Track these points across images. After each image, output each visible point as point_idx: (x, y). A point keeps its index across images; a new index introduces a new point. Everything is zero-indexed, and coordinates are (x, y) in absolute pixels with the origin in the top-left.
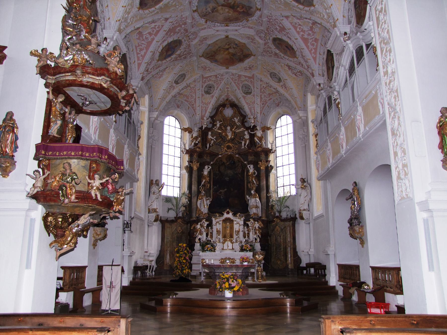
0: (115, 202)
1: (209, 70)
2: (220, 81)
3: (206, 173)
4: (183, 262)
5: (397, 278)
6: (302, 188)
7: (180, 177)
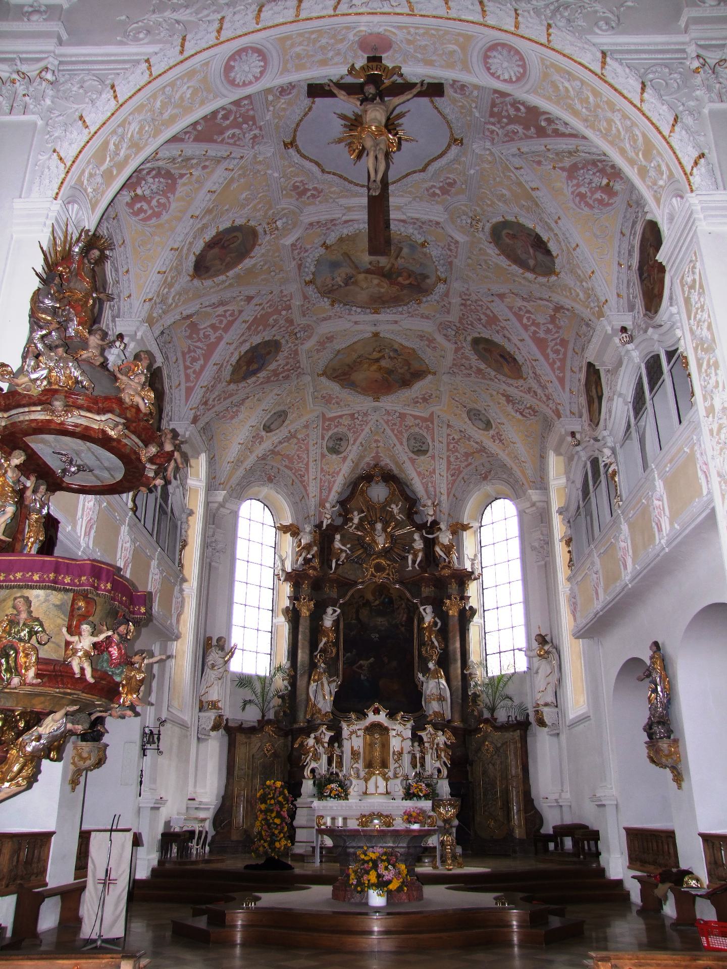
1: (338, 403)
2: (361, 425)
4: (275, 824)
6: (540, 656)
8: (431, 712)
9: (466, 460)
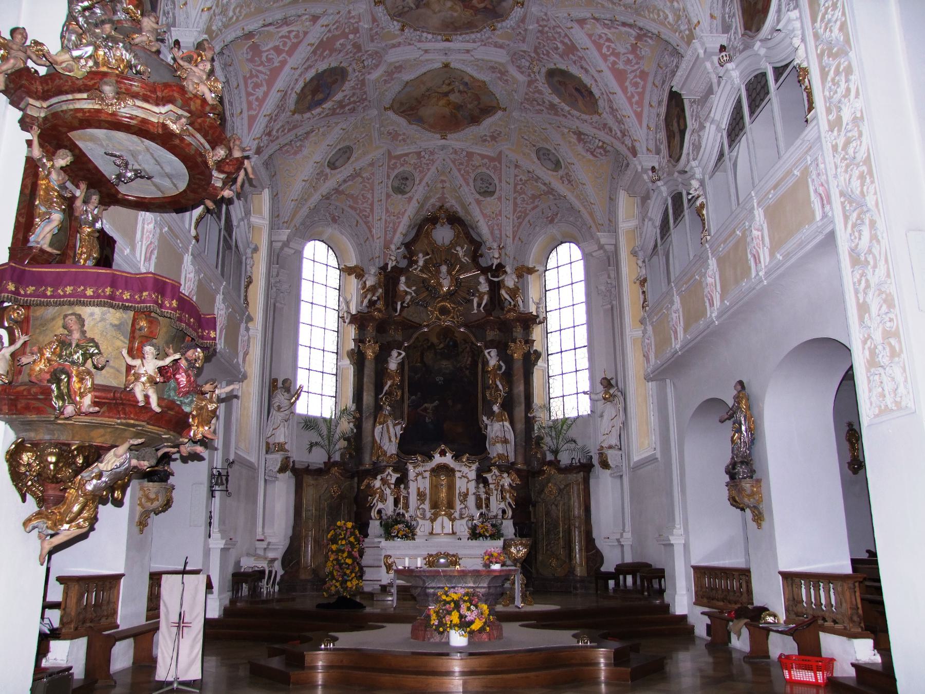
0: (194, 417)
1: (404, 140)
2: (428, 165)
3: (393, 365)
4: (347, 564)
5: (851, 598)
6: (605, 399)
7: (336, 375)
8: (495, 455)
9: (533, 203)
